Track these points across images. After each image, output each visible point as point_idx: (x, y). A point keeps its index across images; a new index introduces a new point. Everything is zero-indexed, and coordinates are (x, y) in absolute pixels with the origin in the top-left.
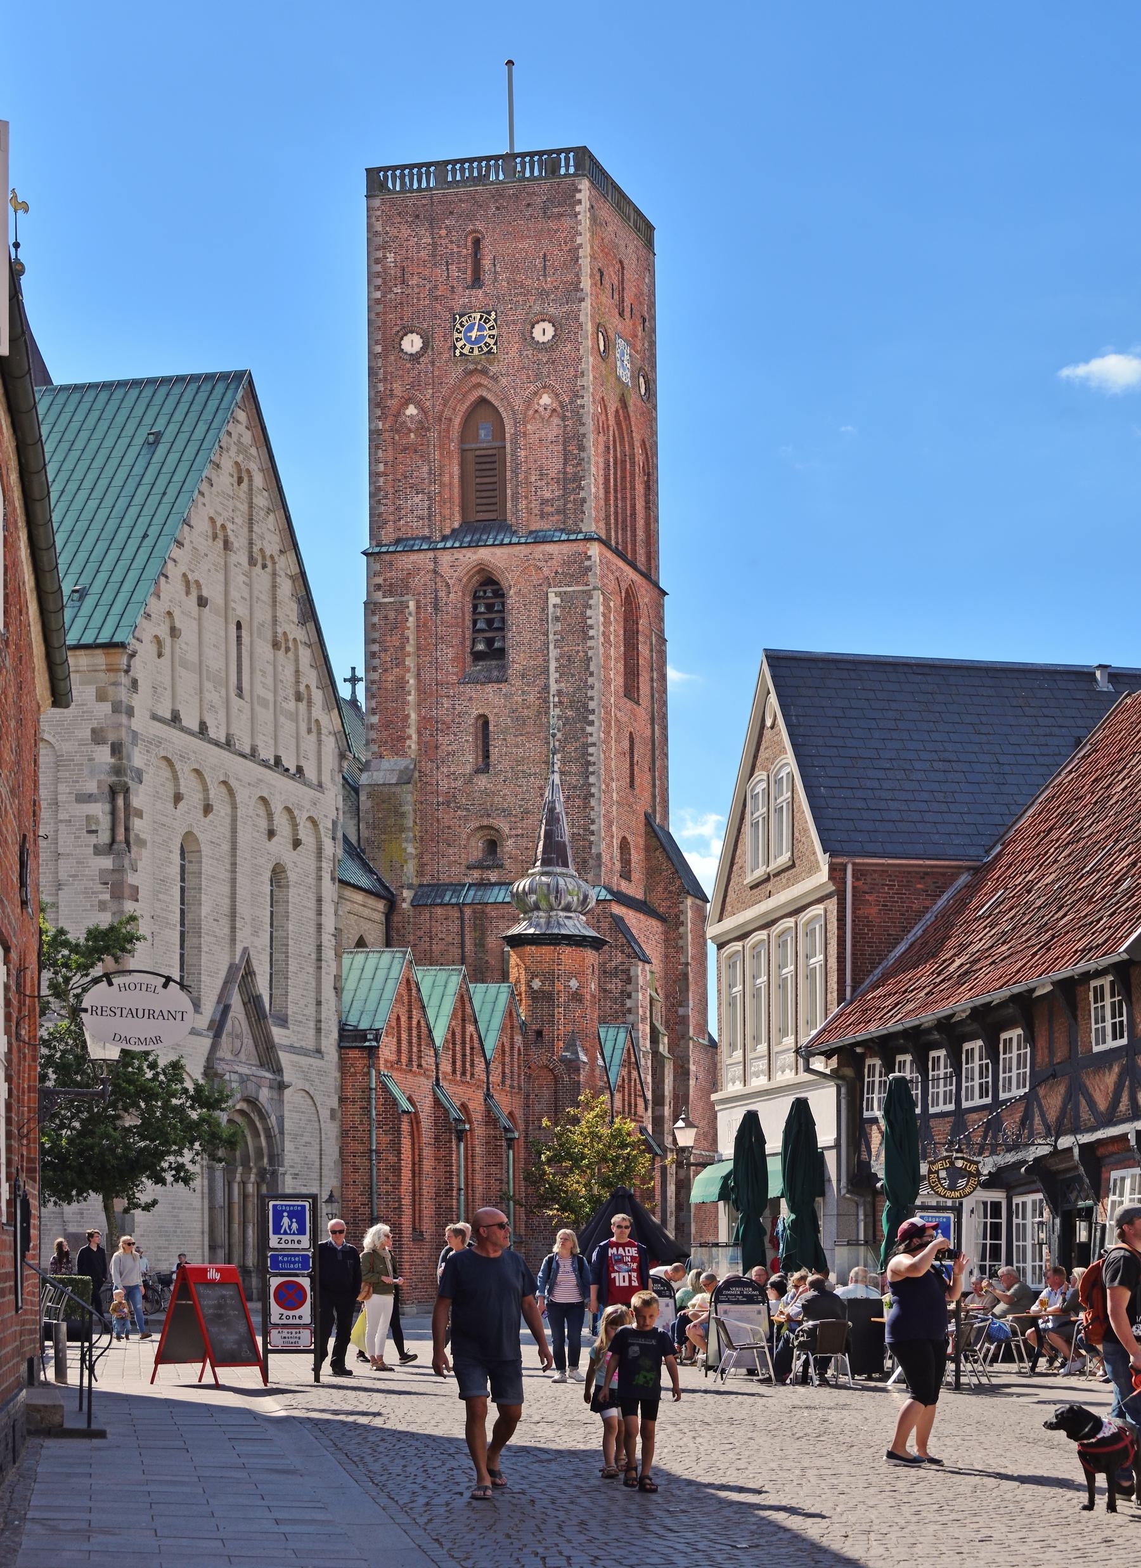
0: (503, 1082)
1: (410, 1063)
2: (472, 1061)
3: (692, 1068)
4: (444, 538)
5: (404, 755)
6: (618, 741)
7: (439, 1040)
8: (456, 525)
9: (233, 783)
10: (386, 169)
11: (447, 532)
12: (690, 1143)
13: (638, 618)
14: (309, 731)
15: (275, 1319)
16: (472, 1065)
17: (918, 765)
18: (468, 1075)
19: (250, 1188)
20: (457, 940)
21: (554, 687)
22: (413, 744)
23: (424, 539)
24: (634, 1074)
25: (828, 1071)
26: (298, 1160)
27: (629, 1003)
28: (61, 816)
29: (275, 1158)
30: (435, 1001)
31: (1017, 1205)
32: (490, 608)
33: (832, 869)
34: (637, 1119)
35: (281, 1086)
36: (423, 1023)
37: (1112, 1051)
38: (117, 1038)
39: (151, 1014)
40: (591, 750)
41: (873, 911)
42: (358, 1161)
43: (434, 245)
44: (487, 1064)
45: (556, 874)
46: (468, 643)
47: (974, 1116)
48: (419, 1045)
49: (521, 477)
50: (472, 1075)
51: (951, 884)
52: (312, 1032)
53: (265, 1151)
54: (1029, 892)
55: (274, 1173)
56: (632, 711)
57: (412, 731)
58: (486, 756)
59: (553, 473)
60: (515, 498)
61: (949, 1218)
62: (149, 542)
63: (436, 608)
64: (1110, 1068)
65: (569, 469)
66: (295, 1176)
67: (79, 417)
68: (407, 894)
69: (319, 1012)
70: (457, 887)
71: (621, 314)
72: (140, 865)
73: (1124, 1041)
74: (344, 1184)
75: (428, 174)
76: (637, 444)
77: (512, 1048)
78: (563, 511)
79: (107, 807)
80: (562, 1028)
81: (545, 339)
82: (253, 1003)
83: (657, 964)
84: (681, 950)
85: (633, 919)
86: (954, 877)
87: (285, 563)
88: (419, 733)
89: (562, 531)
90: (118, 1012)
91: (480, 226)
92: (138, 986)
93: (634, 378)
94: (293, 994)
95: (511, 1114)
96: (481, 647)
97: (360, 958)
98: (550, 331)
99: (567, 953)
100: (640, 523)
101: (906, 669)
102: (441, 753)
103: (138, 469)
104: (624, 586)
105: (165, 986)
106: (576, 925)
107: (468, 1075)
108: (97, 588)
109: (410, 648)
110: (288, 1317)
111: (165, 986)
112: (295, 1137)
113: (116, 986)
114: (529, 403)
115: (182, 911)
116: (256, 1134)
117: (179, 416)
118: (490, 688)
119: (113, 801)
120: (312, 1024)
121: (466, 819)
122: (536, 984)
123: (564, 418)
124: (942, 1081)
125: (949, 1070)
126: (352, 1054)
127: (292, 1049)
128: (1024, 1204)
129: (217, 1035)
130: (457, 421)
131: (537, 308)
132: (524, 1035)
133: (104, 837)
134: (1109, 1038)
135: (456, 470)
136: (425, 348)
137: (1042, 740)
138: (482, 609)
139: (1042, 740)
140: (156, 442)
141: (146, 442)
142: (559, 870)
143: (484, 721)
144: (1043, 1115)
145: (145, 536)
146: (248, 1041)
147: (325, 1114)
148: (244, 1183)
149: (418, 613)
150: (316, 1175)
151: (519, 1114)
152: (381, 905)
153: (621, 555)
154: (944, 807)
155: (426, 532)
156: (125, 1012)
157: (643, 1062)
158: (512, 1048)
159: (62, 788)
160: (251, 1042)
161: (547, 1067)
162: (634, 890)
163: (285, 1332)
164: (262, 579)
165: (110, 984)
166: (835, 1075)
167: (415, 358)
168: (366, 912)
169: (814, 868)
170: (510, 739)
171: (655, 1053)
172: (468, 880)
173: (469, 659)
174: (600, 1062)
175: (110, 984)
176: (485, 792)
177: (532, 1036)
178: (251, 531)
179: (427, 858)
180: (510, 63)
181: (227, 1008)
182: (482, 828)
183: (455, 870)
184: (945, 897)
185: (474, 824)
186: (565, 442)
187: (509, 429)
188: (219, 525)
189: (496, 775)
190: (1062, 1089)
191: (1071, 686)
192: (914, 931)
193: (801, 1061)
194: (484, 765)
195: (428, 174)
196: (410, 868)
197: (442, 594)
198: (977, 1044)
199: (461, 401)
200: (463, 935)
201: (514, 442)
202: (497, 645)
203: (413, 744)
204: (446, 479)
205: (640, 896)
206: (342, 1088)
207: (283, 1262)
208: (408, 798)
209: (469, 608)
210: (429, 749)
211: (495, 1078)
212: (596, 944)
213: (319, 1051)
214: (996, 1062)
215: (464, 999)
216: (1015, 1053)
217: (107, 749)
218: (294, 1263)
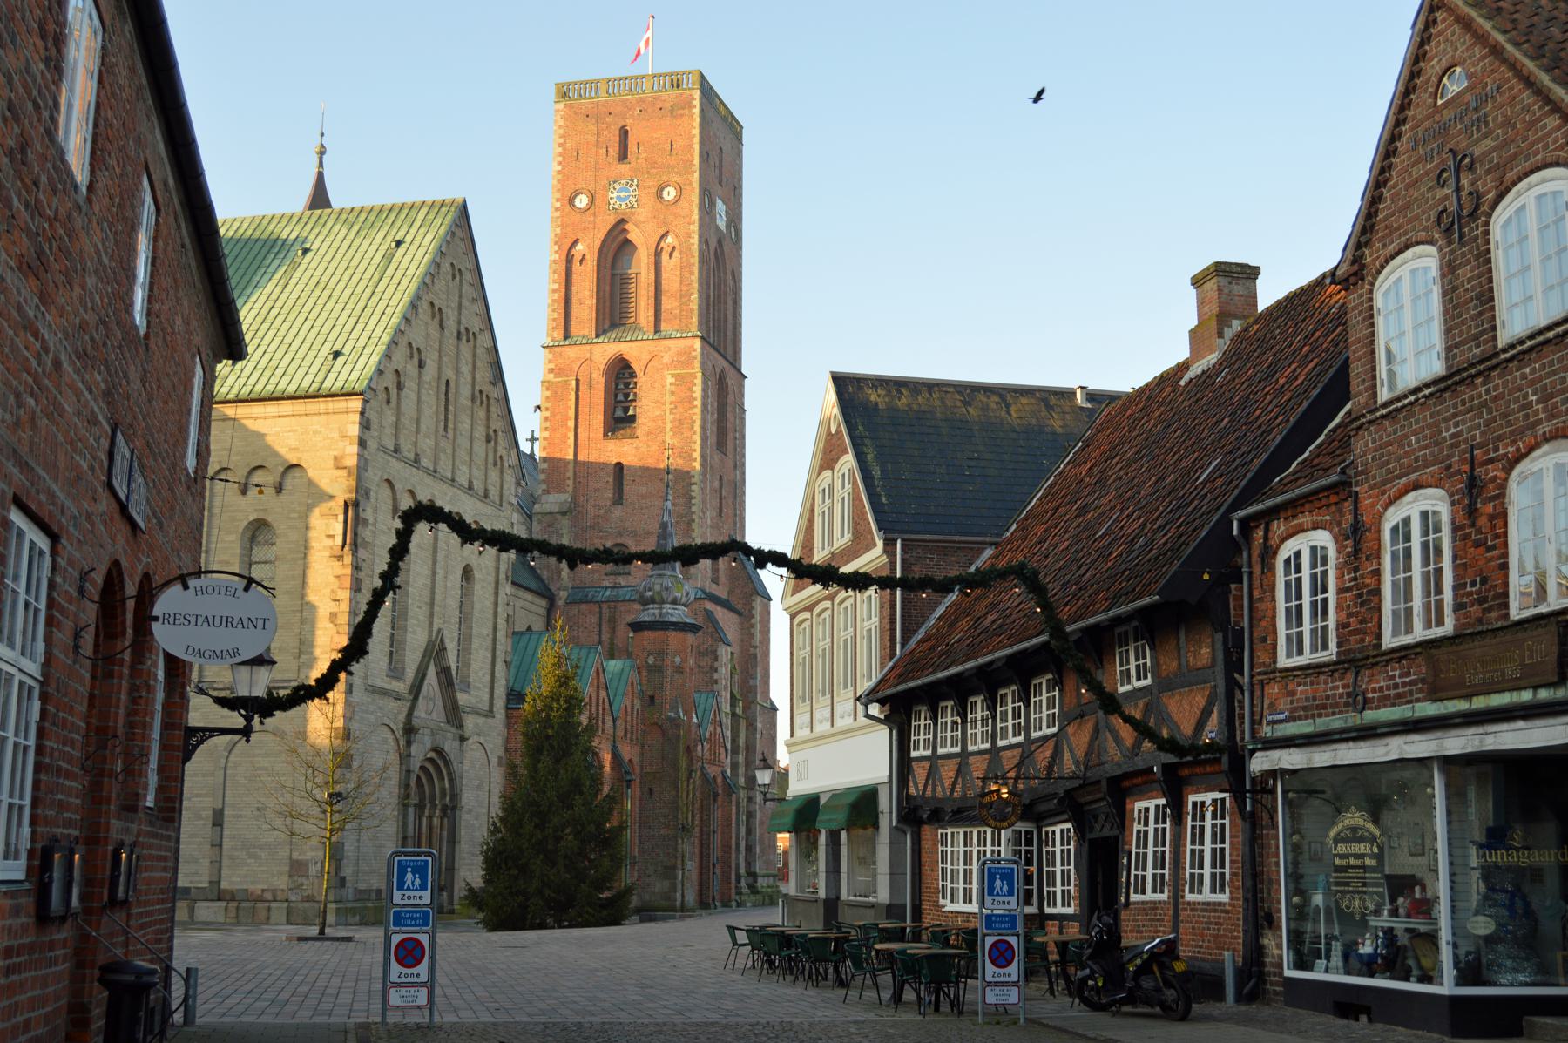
0: (625, 735)
3: (759, 725)
5: (564, 492)
6: (712, 482)
12: (767, 781)
13: (727, 394)
14: (495, 464)
15: (394, 978)
19: (436, 821)
24: (719, 730)
25: (882, 717)
27: (716, 676)
29: (455, 797)
31: (1047, 833)
33: (886, 544)
34: (720, 763)
35: (463, 739)
37: (1135, 690)
38: (191, 650)
39: (229, 622)
40: (693, 487)
47: (1008, 753)
53: (448, 792)
54: (1046, 557)
56: (722, 460)
65: (684, 289)
68: (564, 594)
71: (720, 184)
73: (1148, 682)
76: (729, 272)
77: (632, 709)
80: (669, 693)
81: (669, 189)
82: (445, 673)
83: (736, 648)
84: (752, 636)
85: (720, 613)
86: (981, 551)
87: (484, 340)
90: (193, 620)
92: (217, 589)
93: (728, 226)
94: (475, 666)
95: (630, 761)
99: (674, 637)
100: (730, 327)
104: (718, 370)
105: (247, 589)
106: (678, 614)
110: (406, 976)
111: (247, 589)
113: (192, 590)
116: (441, 778)
122: (651, 660)
124: (979, 723)
125: (986, 713)
129: (416, 698)
132: (642, 700)
134: (1133, 679)
138: (621, 386)
146: (439, 703)
147: (494, 760)
148: (431, 817)
151: (636, 760)
152: (544, 603)
153: (715, 349)
156: (200, 620)
157: (724, 720)
158: (632, 709)
160: (441, 704)
161: (656, 724)
162: (721, 592)
163: (403, 991)
164: (465, 349)
165: (186, 587)
166: (887, 721)
168: (534, 608)
169: (871, 545)
171: (734, 714)
174: (695, 720)
175: (186, 587)
178: (460, 314)
181: (424, 676)
193: (860, 708)
202: (631, 412)
205: (724, 596)
206: (507, 741)
207: (405, 918)
211: (620, 733)
212: (694, 628)
214: (1027, 705)
216: (1045, 696)
218: (416, 919)
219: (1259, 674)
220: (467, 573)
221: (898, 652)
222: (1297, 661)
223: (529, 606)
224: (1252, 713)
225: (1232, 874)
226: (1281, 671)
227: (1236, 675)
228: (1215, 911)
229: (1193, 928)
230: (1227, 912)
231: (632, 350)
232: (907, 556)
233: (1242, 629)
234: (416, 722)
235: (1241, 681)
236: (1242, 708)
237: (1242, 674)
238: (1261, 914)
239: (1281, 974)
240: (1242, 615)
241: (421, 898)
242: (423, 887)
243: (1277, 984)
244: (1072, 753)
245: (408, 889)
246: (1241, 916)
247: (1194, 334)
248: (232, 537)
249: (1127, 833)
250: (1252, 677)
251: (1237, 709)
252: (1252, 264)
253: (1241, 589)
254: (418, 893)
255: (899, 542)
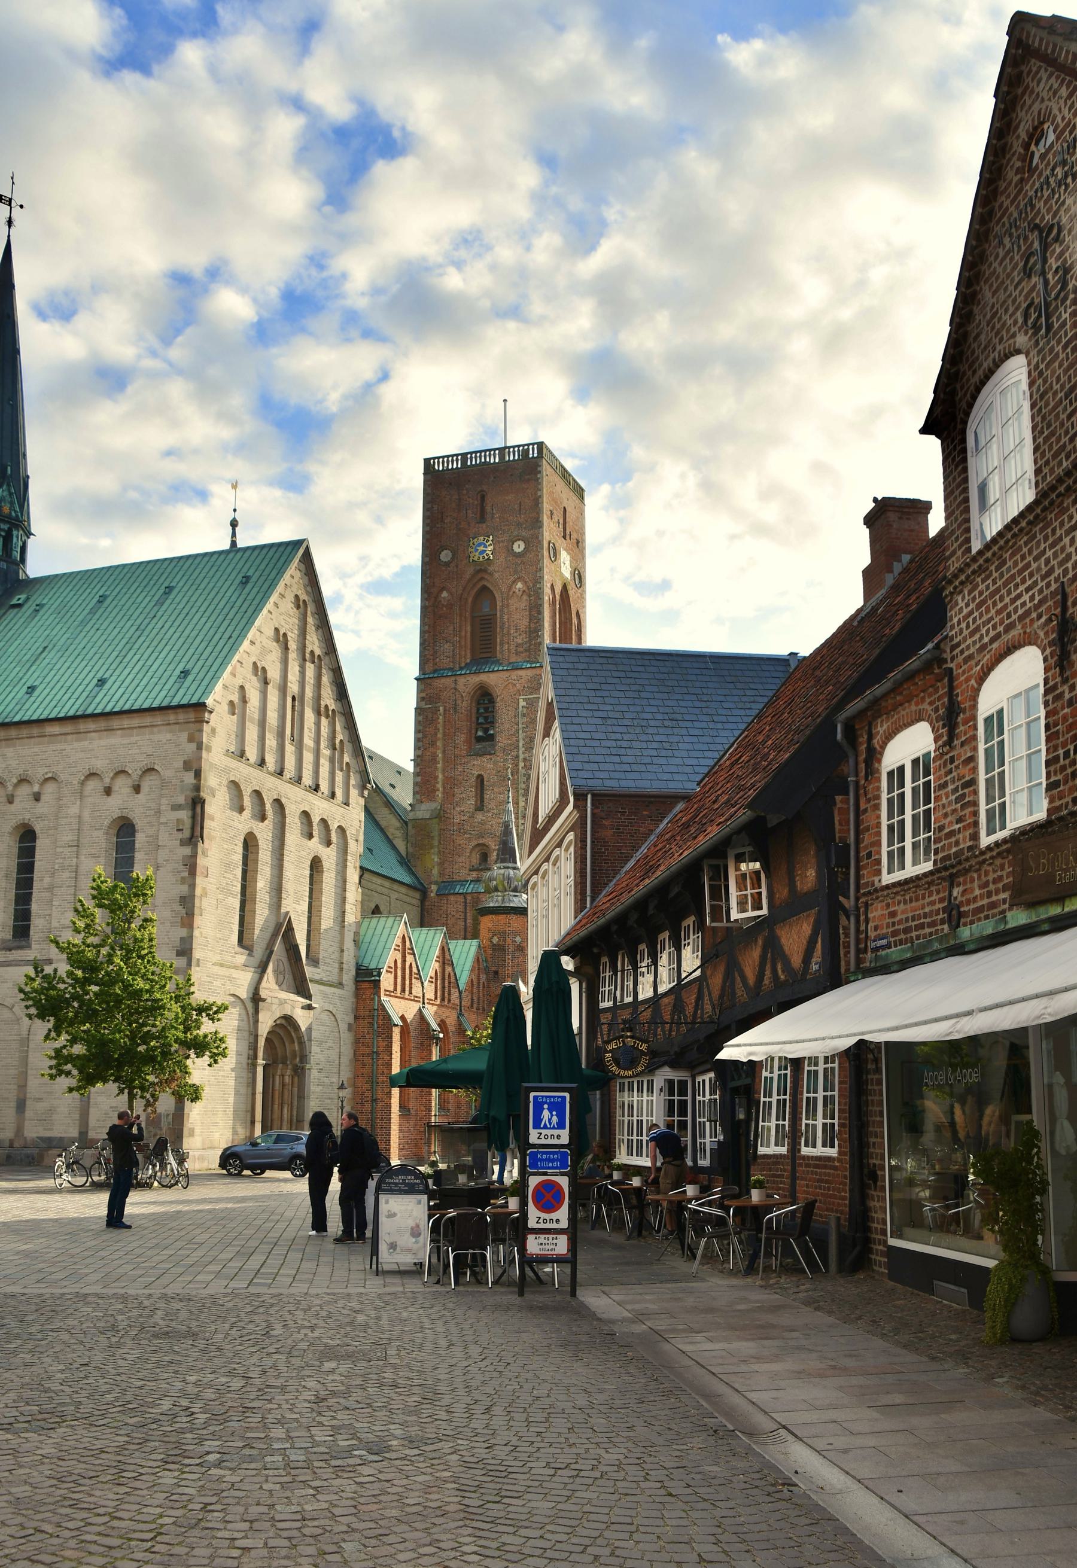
0: (472, 1005)
1: (403, 990)
2: (450, 991)
4: (461, 669)
5: (435, 800)
7: (462, 986)
8: (468, 661)
9: (283, 800)
10: (434, 458)
11: (463, 665)
16: (449, 994)
17: (652, 723)
18: (407, 992)
19: (287, 1079)
20: (463, 915)
21: (521, 757)
22: (439, 794)
23: (451, 669)
26: (323, 1059)
28: (162, 820)
29: (304, 1058)
30: (462, 962)
32: (486, 709)
36: (414, 965)
41: (608, 833)
42: (366, 1059)
43: (460, 499)
44: (460, 993)
45: (508, 868)
46: (473, 731)
48: (411, 980)
49: (505, 631)
50: (411, 993)
51: (670, 811)
52: (337, 970)
55: (303, 1069)
57: (439, 786)
58: (482, 801)
59: (523, 628)
60: (502, 644)
61: (564, 1098)
62: (232, 641)
63: (455, 711)
64: (756, 941)
65: (532, 625)
66: (320, 1070)
67: (205, 570)
68: (434, 887)
69: (342, 957)
70: (462, 882)
72: (210, 853)
74: (356, 1076)
75: (457, 460)
78: (528, 650)
79: (190, 813)
81: (520, 550)
82: (292, 949)
88: (444, 788)
89: (528, 662)
91: (485, 488)
93: (573, 573)
96: (480, 733)
97: (374, 921)
98: (522, 546)
101: (651, 657)
102: (456, 799)
103: (233, 599)
107: (407, 992)
108: (195, 671)
109: (440, 735)
112: (321, 1043)
114: (510, 588)
115: (310, 904)
117: (262, 567)
118: (485, 759)
119: (194, 809)
120: (337, 965)
121: (470, 839)
122: (495, 940)
123: (529, 596)
126: (364, 986)
127: (320, 982)
128: (704, 1081)
130: (470, 600)
131: (515, 533)
132: (487, 974)
133: (187, 834)
135: (469, 628)
136: (453, 558)
137: (748, 705)
138: (482, 711)
139: (748, 705)
140: (246, 583)
141: (241, 582)
142: (510, 865)
143: (480, 779)
144: (710, 995)
145: (230, 637)
147: (343, 1027)
149: (445, 714)
150: (335, 1070)
154: (670, 753)
155: (451, 665)
158: (479, 983)
159: (164, 801)
167: (447, 564)
168: (408, 899)
170: (495, 788)
172: (470, 878)
173: (473, 740)
176: (483, 823)
177: (492, 975)
179: (446, 864)
180: (505, 401)
182: (479, 845)
183: (463, 872)
184: (666, 821)
185: (474, 843)
186: (530, 610)
187: (499, 604)
188: (281, 633)
189: (488, 811)
190: (722, 969)
191: (771, 668)
192: (641, 850)
194: (480, 807)
195: (457, 460)
196: (435, 871)
197: (459, 702)
198: (665, 935)
199: (472, 588)
200: (466, 913)
201: (502, 611)
203: (439, 794)
204: (463, 634)
208: (435, 826)
209: (474, 710)
210: (449, 796)
211: (466, 1003)
213: (341, 984)
215: (444, 950)
217: (192, 774)
219: (864, 895)
220: (316, 865)
221: (588, 905)
222: (898, 876)
223: (404, 898)
224: (858, 941)
225: (840, 1125)
226: (887, 887)
227: (841, 898)
228: (825, 1167)
229: (807, 1186)
230: (835, 1168)
231: (493, 679)
232: (596, 811)
233: (849, 846)
234: (263, 994)
235: (847, 906)
236: (847, 935)
237: (848, 897)
238: (866, 1171)
239: (886, 1241)
240: (849, 830)
241: (559, 1137)
242: (561, 1125)
243: (883, 1254)
244: (710, 995)
245: (545, 1127)
246: (848, 1173)
247: (867, 573)
248: (100, 833)
249: (757, 1080)
250: (857, 899)
251: (842, 937)
252: (923, 498)
253: (847, 802)
254: (556, 1132)
255: (589, 796)
